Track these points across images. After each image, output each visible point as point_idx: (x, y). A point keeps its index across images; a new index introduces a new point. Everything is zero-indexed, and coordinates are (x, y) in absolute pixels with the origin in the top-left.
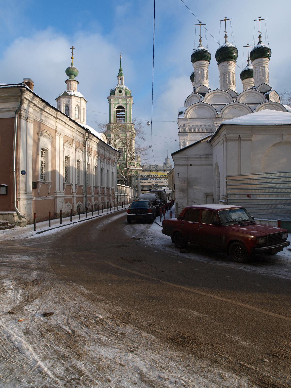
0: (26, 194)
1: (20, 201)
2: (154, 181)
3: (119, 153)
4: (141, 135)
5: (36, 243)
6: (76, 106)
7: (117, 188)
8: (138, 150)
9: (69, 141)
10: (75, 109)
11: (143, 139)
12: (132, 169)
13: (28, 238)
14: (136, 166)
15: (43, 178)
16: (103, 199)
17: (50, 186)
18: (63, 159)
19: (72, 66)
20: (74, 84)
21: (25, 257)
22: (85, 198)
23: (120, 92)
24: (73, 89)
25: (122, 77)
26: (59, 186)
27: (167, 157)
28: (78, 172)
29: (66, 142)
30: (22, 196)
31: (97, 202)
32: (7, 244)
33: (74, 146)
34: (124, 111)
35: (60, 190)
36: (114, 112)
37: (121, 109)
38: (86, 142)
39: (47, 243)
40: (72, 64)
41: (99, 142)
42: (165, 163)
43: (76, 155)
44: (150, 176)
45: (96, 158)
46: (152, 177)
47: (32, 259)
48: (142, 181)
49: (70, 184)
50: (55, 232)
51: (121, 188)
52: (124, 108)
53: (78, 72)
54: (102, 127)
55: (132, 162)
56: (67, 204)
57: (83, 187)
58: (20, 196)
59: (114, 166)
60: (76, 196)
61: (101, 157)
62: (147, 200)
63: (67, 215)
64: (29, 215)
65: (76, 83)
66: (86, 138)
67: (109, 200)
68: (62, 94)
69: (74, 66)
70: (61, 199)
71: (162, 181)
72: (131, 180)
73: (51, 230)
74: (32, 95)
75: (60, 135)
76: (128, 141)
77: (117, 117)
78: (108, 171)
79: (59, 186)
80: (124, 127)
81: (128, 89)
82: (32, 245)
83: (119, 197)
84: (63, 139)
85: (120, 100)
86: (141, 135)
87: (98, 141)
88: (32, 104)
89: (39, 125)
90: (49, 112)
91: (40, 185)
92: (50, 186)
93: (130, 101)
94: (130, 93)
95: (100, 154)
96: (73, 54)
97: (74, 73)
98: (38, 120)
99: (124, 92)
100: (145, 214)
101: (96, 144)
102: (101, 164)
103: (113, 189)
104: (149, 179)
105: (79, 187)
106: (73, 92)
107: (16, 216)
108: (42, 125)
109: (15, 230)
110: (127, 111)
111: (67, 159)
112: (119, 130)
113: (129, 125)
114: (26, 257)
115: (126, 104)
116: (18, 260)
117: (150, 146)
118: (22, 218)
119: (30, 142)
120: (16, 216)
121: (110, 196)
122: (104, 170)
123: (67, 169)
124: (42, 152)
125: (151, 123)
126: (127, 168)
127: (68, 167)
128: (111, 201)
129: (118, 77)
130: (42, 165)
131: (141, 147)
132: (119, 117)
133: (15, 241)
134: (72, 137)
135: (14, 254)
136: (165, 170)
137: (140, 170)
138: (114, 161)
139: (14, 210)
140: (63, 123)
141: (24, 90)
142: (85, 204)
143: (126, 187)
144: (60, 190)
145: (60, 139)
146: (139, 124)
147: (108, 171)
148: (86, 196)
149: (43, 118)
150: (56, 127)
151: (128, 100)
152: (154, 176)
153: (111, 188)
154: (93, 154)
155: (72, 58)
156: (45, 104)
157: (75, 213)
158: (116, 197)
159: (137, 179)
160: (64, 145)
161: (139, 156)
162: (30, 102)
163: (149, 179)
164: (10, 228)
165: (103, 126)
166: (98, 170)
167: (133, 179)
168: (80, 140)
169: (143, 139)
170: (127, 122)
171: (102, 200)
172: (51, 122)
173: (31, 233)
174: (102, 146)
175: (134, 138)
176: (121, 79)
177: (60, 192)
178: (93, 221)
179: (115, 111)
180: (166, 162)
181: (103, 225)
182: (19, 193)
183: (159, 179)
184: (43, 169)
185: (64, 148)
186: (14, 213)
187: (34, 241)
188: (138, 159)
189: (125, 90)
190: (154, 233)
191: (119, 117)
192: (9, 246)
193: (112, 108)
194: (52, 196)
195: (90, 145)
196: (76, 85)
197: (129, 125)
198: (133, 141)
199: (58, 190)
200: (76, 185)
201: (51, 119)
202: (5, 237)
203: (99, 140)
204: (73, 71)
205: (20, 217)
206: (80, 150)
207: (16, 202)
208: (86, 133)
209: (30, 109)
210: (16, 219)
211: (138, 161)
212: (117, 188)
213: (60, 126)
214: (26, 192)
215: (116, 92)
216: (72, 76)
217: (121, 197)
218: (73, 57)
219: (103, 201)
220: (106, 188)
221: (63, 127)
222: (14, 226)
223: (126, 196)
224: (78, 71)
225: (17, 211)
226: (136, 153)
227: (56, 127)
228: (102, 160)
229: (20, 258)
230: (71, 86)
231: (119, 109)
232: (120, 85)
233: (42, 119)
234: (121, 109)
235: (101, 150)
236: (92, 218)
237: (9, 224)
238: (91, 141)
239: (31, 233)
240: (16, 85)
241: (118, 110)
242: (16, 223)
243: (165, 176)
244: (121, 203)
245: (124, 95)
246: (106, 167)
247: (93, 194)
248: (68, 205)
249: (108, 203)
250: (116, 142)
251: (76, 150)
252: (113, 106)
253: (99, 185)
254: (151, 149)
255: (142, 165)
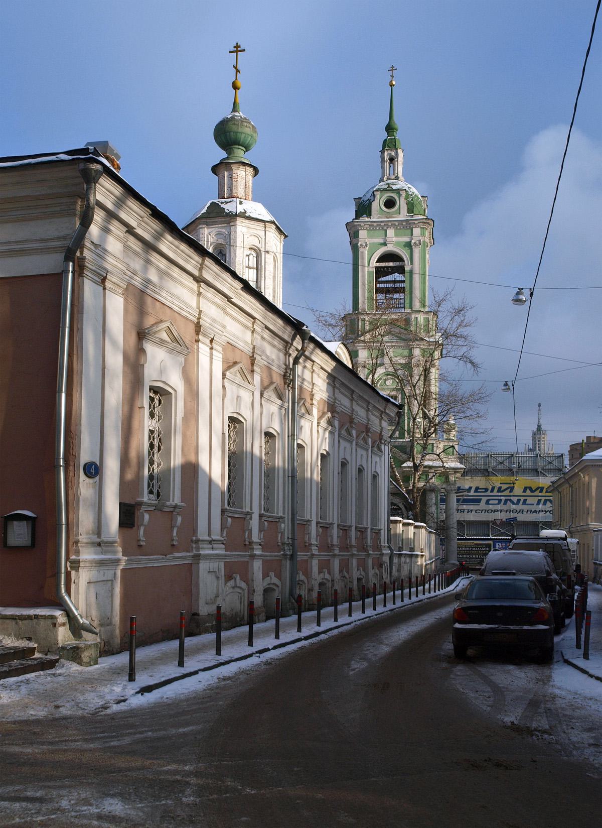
0: (99, 545)
1: (77, 571)
2: (499, 507)
3: (396, 410)
4: (464, 349)
5: (141, 733)
6: (249, 252)
7: (389, 530)
8: (450, 403)
9: (241, 364)
10: (246, 263)
11: (471, 362)
12: (430, 467)
13: (109, 711)
14: (442, 455)
15: (155, 491)
16: (345, 566)
17: (179, 519)
18: (220, 424)
19: (237, 114)
20: (242, 176)
21: (111, 801)
22: (288, 562)
23: (390, 204)
24: (240, 191)
25: (397, 154)
26: (209, 521)
27: (539, 427)
28: (269, 473)
29: (229, 368)
30: (87, 555)
31: (327, 576)
32: (35, 733)
33: (257, 378)
34: (401, 270)
35: (209, 535)
36: (370, 273)
37: (391, 264)
38: (293, 370)
39: (184, 735)
40: (235, 108)
41: (334, 369)
42: (531, 447)
43: (263, 413)
44: (486, 490)
45: (323, 423)
46: (495, 493)
47: (141, 814)
48: (460, 507)
49: (242, 513)
50: (200, 687)
51: (400, 528)
52: (402, 260)
53: (254, 135)
54: (330, 325)
55: (430, 442)
56: (231, 583)
57: (283, 525)
58: (77, 553)
59: (380, 453)
60: (261, 555)
61: (341, 422)
62: (514, 574)
63: (235, 622)
64: (106, 622)
65: (250, 171)
66: (294, 354)
67: (365, 569)
68: (204, 211)
69: (240, 114)
70: (214, 565)
71: (529, 507)
72: (424, 503)
73: (187, 679)
74: (117, 190)
75: (211, 341)
76: (418, 371)
77: (378, 290)
78: (360, 471)
79: (209, 521)
80: (402, 324)
81: (416, 192)
82: (127, 740)
83: (395, 560)
84: (221, 356)
85: (388, 231)
86: (464, 349)
87: (330, 365)
88: (116, 223)
89: (140, 299)
90: (171, 255)
91: (147, 517)
92: (179, 519)
93: (423, 235)
94: (424, 206)
95: (338, 413)
96: (237, 71)
97: (242, 138)
98: (137, 282)
99: (402, 204)
100: (525, 627)
101: (324, 375)
102: (339, 447)
103: (377, 533)
104: (484, 499)
105: (270, 522)
106: (241, 203)
107: (64, 624)
108: (149, 301)
109: (60, 675)
110: (411, 272)
111: (232, 426)
112: (388, 334)
113: (421, 318)
114: (114, 801)
115: (409, 245)
116: (85, 817)
117: (506, 384)
118: (84, 633)
119: (115, 361)
120: (64, 624)
121: (369, 555)
122: (349, 466)
123: (236, 461)
124: (152, 399)
125: (532, 294)
126: (414, 464)
127: (234, 453)
128: (371, 572)
129: (382, 152)
130: (152, 446)
131: (461, 392)
132: (387, 291)
133: (63, 722)
134: (248, 349)
135: (66, 782)
136: (540, 470)
137: (455, 470)
138: (381, 437)
139: (60, 604)
140: (219, 299)
141: (96, 171)
142: (288, 584)
143: (416, 527)
144: (209, 535)
145: (211, 354)
146: (459, 311)
147: (360, 471)
148: (292, 557)
149: (153, 276)
150: (200, 314)
151: (417, 231)
152: (499, 490)
153: (369, 530)
154: (315, 412)
155: (235, 87)
156: (160, 225)
157: (259, 614)
158: (386, 559)
159: (443, 501)
160: (224, 376)
161: (452, 422)
162: (111, 215)
163: (484, 499)
164: (42, 670)
165: (333, 322)
166: (331, 467)
167: (432, 498)
168: (273, 361)
169: (471, 362)
170: (411, 307)
171: (341, 571)
172: (180, 294)
173: (118, 689)
174: (343, 384)
175: (437, 363)
176: (392, 160)
177: (210, 542)
178: (323, 645)
179: (371, 269)
180: (534, 444)
181: (366, 664)
182: (77, 542)
183: (519, 500)
184: (156, 458)
185: (224, 387)
186: (58, 613)
187: (132, 726)
188: (450, 431)
189: (406, 198)
190: (582, 708)
191: (387, 291)
192: (43, 743)
193: (363, 261)
194: (184, 554)
195: (303, 379)
196: (250, 178)
197: (421, 318)
198: (433, 370)
199: (202, 534)
200: (261, 516)
201: (181, 284)
202: (26, 706)
203: (334, 364)
204: (240, 130)
205: (76, 628)
206: (274, 398)
207: (63, 575)
208: (293, 338)
209: (110, 245)
210: (63, 635)
211: (449, 439)
212: (389, 530)
213: (212, 310)
214: (99, 540)
215: (375, 206)
216: (236, 150)
217: (403, 559)
218: (239, 83)
219: (346, 574)
220: (356, 528)
221: (222, 312)
222: (57, 661)
223: (417, 556)
224: (255, 132)
225: (68, 605)
226: (444, 412)
227: (200, 314)
228: (343, 432)
229: (91, 805)
230: (234, 183)
231: (387, 264)
232: (388, 179)
233: (148, 281)
234: (391, 263)
235: (339, 396)
236: (317, 634)
237: (37, 655)
238: (309, 364)
239: (118, 689)
240: (68, 153)
241: (383, 267)
242: (63, 648)
243: (541, 492)
244: (413, 580)
245: (403, 215)
246: (358, 457)
247: (315, 551)
248: (233, 588)
249: (359, 580)
250: (376, 376)
251: (262, 395)
252: (364, 253)
253: (333, 517)
254: (510, 393)
255: (464, 451)
